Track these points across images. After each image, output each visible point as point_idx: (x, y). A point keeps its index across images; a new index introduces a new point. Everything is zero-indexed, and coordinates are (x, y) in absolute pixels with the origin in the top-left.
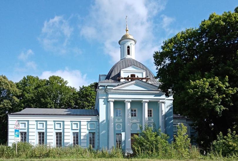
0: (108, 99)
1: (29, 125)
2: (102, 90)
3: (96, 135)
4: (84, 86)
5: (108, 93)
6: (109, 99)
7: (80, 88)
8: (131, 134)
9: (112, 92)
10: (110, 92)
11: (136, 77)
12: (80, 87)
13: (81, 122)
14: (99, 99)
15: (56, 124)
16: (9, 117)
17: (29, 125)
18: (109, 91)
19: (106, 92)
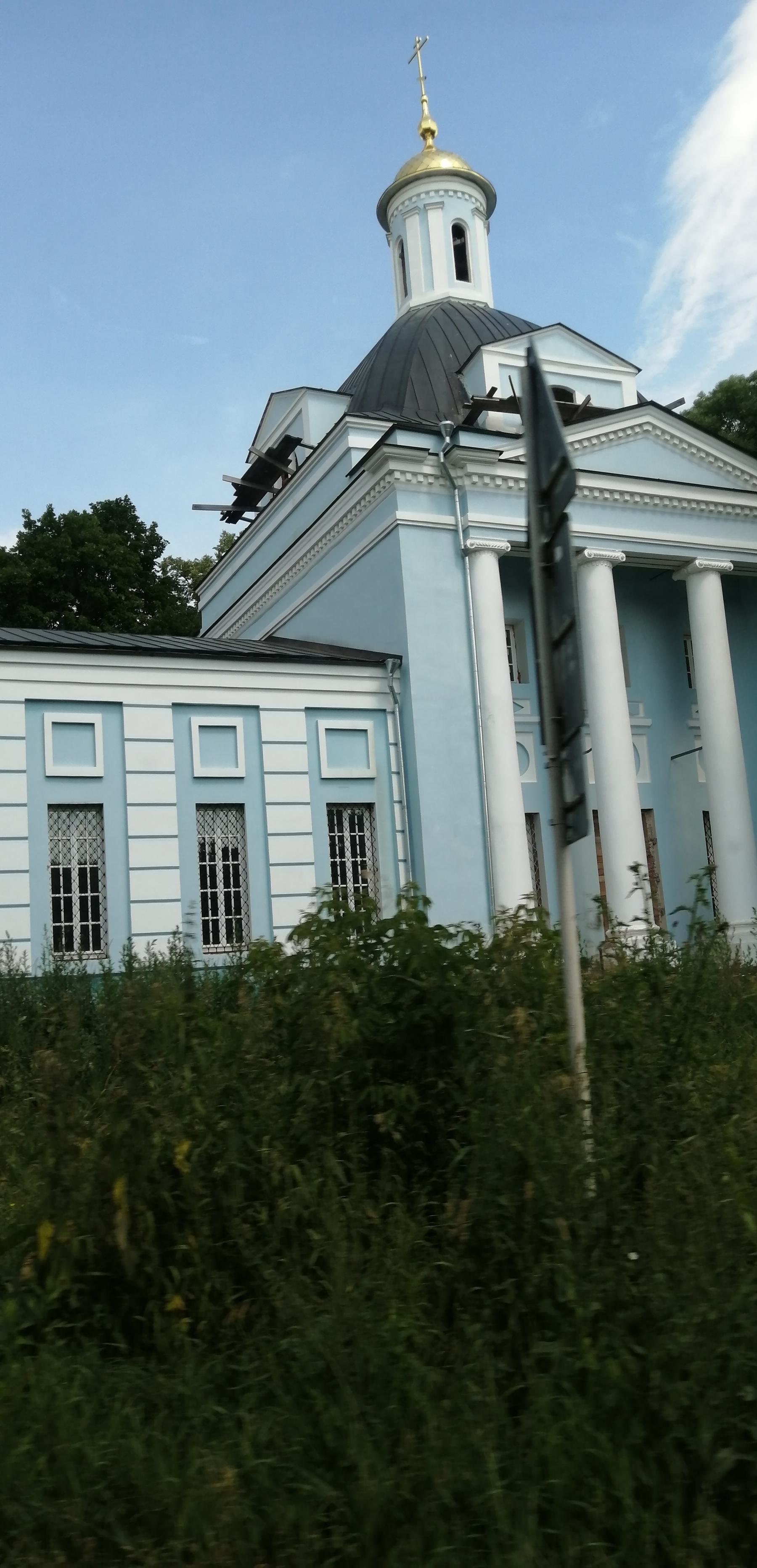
0: (466, 530)
1: (266, 776)
2: (420, 462)
3: (387, 827)
4: (57, 513)
5: (461, 488)
6: (472, 533)
7: (50, 513)
8: (642, 810)
9: (505, 479)
10: (493, 477)
11: (579, 400)
12: (27, 515)
13: (125, 708)
14: (395, 527)
15: (48, 727)
16: (570, 439)
17: (263, 773)
18: (471, 468)
19: (451, 480)
